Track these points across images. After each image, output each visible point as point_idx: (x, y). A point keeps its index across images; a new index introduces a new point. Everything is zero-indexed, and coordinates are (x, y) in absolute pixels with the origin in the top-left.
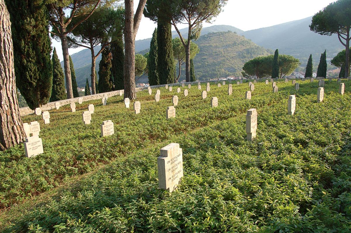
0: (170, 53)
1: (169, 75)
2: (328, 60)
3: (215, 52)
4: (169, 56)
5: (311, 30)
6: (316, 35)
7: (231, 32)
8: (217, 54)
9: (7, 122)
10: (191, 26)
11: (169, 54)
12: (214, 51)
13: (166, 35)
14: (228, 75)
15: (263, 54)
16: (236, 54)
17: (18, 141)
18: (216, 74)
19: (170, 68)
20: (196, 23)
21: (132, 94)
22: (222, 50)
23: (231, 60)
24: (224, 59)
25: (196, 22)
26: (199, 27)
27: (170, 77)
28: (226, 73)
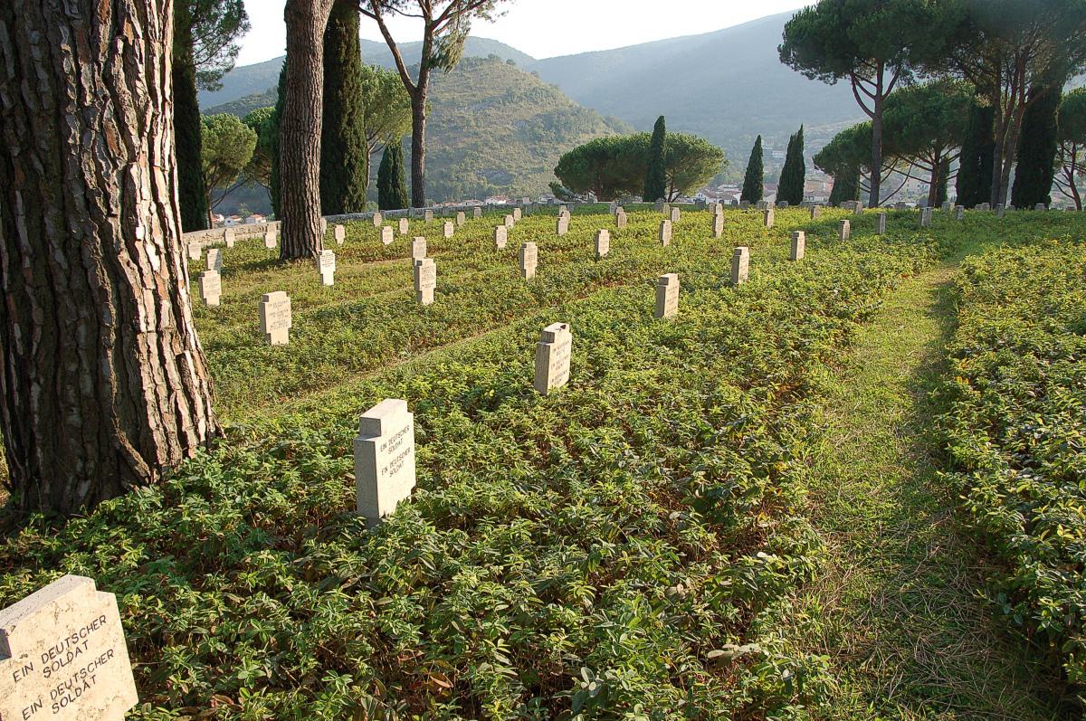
0: (354, 110)
1: (350, 183)
2: (808, 155)
3: (449, 121)
4: (350, 123)
5: (782, 61)
6: (793, 77)
7: (498, 58)
8: (456, 128)
9: (157, 331)
10: (431, 26)
11: (350, 114)
12: (446, 115)
13: (343, 51)
14: (489, 194)
15: (593, 132)
16: (511, 128)
17: (202, 431)
18: (451, 189)
19: (353, 160)
20: (450, 15)
21: (312, 239)
22: (469, 115)
23: (497, 145)
24: (476, 144)
25: (450, 12)
26: (460, 29)
27: (355, 191)
28: (482, 187)
